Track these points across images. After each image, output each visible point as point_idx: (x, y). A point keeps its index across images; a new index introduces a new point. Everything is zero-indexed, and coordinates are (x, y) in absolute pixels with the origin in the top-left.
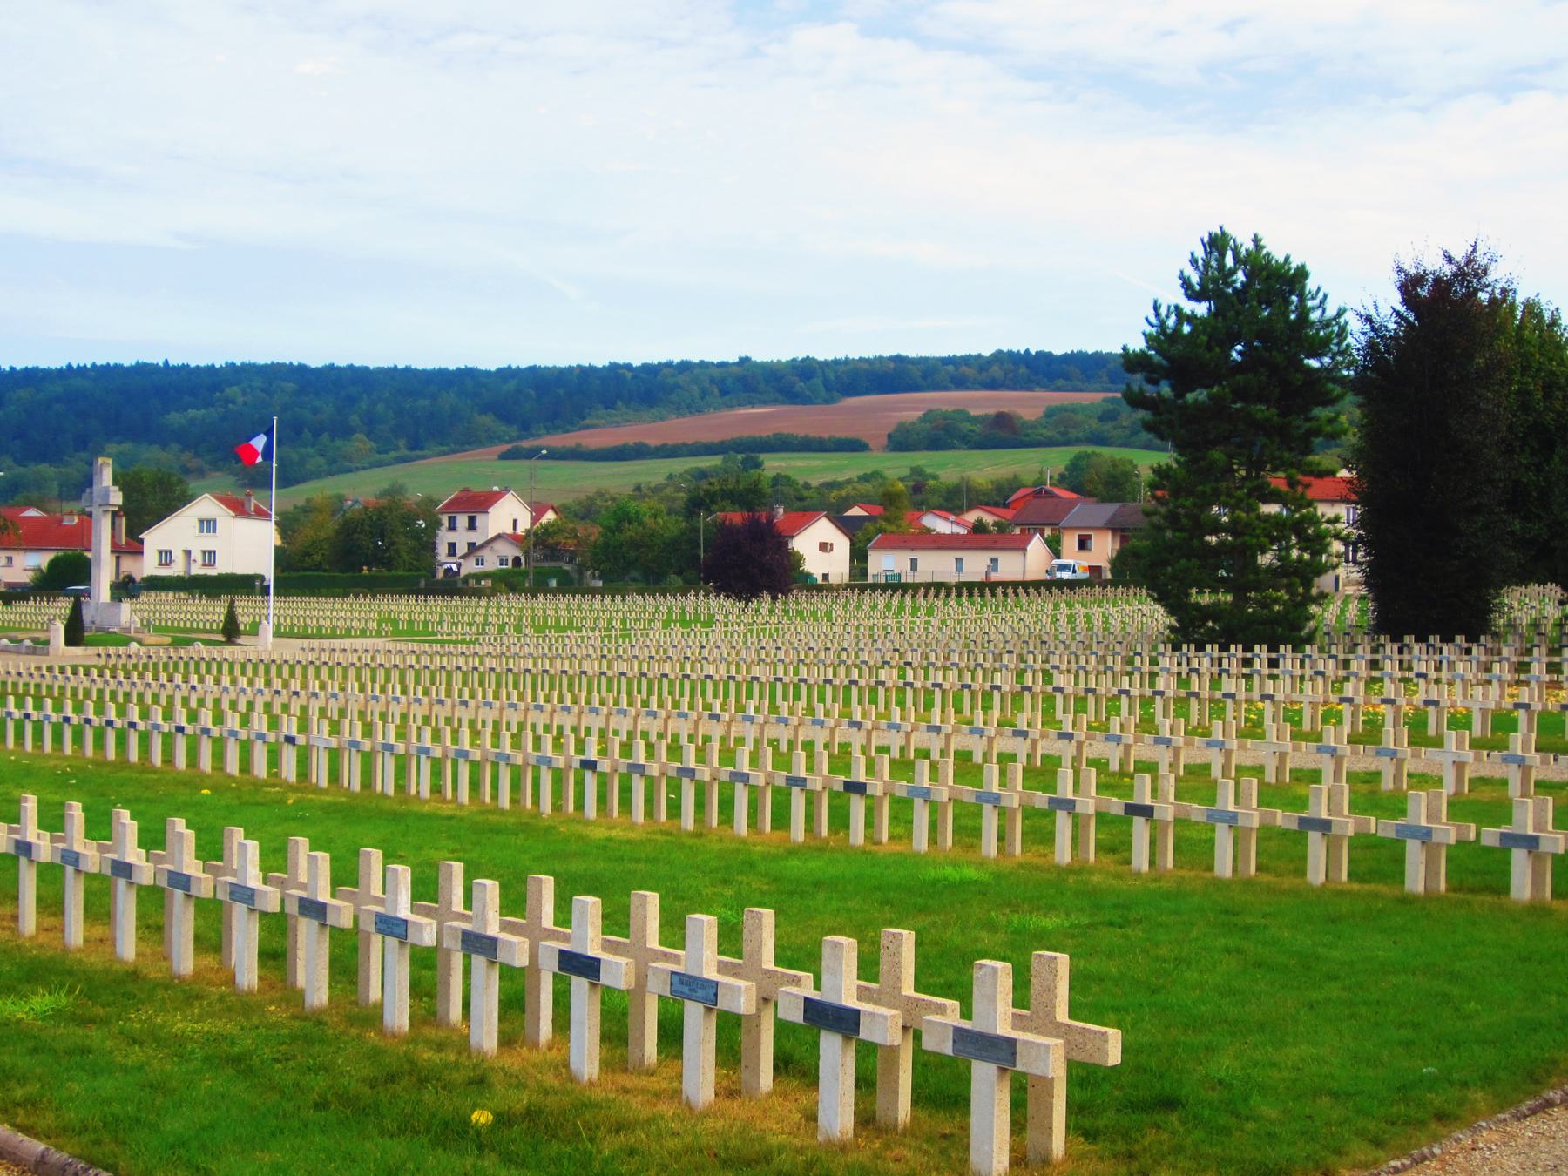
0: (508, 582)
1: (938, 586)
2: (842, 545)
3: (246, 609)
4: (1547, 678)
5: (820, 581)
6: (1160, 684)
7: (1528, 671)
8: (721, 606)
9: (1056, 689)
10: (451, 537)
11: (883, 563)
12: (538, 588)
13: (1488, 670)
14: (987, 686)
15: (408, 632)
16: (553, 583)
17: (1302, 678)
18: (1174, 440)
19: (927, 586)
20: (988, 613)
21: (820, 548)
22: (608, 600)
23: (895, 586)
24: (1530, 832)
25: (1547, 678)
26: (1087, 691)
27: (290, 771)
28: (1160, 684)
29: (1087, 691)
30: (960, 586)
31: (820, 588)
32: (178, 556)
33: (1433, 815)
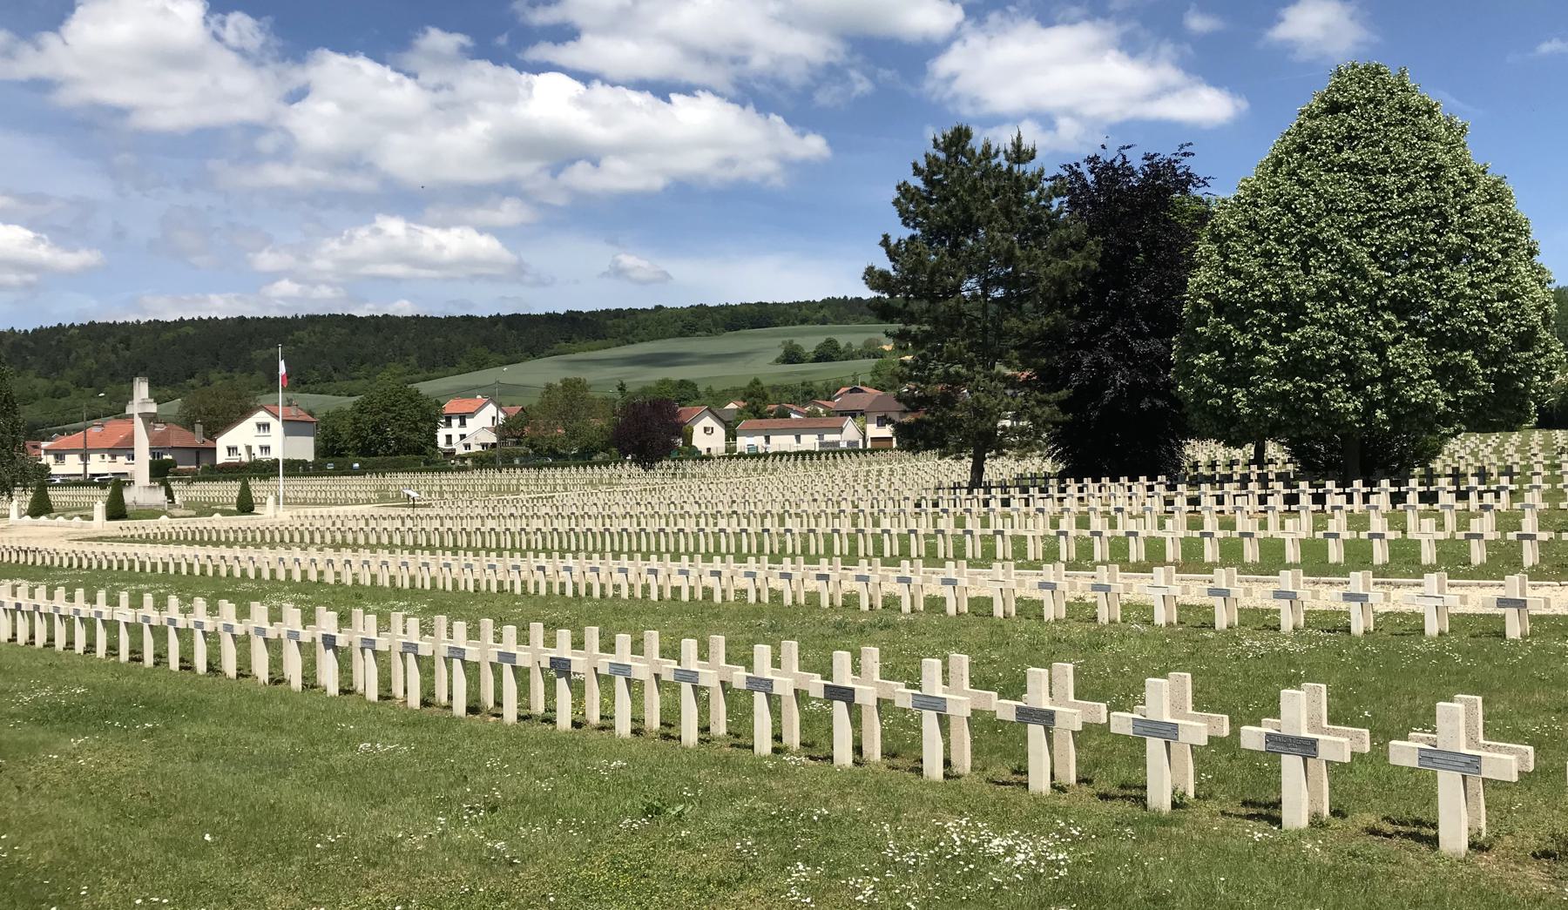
0: (485, 460)
1: (782, 454)
2: (720, 432)
3: (257, 487)
4: (1188, 508)
5: (704, 453)
6: (942, 524)
7: (1297, 502)
8: (628, 472)
9: (1093, 534)
10: (448, 431)
11: (743, 443)
12: (507, 462)
13: (1171, 503)
14: (829, 530)
15: (383, 498)
16: (517, 462)
17: (1027, 515)
18: (1463, 421)
19: (775, 454)
20: (812, 472)
21: (707, 435)
22: (574, 469)
23: (755, 455)
24: (1305, 734)
25: (1188, 508)
26: (810, 531)
27: (329, 675)
28: (942, 524)
29: (810, 531)
30: (797, 454)
31: (702, 458)
32: (242, 450)
33: (1176, 707)
